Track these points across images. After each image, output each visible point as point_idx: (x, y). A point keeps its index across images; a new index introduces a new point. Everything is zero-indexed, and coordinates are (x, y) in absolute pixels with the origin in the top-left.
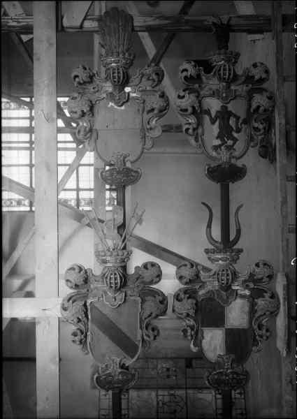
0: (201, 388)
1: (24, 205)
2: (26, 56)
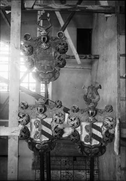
0: (80, 170)
1: (5, 89)
2: (8, 23)
